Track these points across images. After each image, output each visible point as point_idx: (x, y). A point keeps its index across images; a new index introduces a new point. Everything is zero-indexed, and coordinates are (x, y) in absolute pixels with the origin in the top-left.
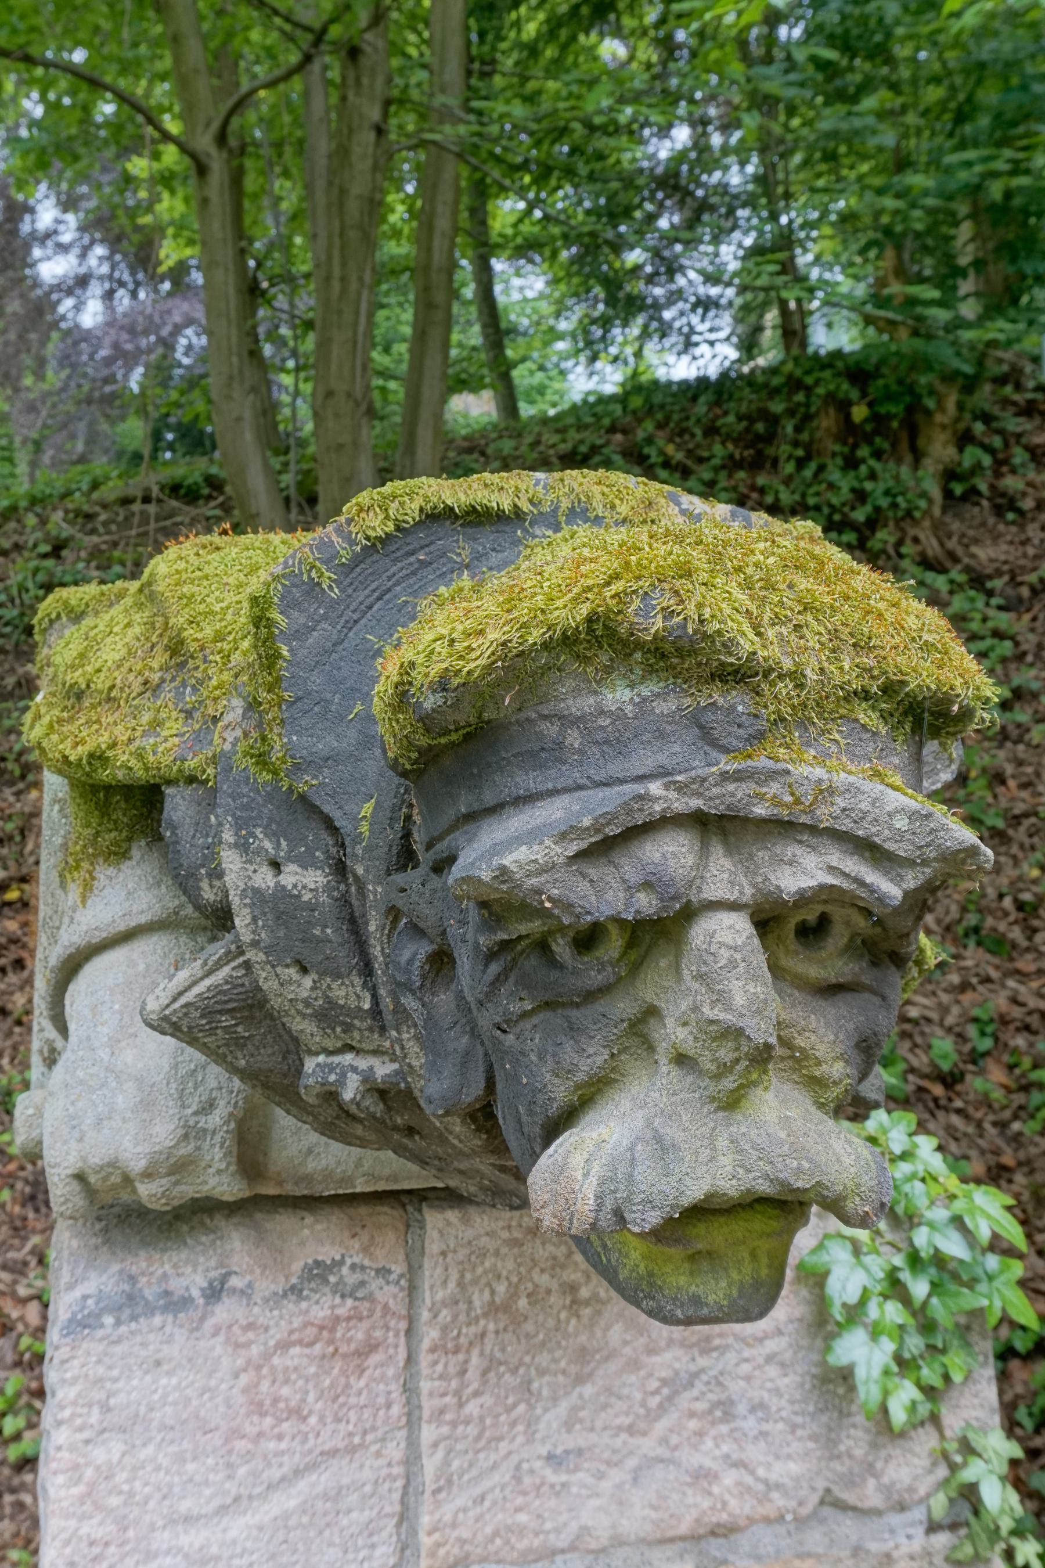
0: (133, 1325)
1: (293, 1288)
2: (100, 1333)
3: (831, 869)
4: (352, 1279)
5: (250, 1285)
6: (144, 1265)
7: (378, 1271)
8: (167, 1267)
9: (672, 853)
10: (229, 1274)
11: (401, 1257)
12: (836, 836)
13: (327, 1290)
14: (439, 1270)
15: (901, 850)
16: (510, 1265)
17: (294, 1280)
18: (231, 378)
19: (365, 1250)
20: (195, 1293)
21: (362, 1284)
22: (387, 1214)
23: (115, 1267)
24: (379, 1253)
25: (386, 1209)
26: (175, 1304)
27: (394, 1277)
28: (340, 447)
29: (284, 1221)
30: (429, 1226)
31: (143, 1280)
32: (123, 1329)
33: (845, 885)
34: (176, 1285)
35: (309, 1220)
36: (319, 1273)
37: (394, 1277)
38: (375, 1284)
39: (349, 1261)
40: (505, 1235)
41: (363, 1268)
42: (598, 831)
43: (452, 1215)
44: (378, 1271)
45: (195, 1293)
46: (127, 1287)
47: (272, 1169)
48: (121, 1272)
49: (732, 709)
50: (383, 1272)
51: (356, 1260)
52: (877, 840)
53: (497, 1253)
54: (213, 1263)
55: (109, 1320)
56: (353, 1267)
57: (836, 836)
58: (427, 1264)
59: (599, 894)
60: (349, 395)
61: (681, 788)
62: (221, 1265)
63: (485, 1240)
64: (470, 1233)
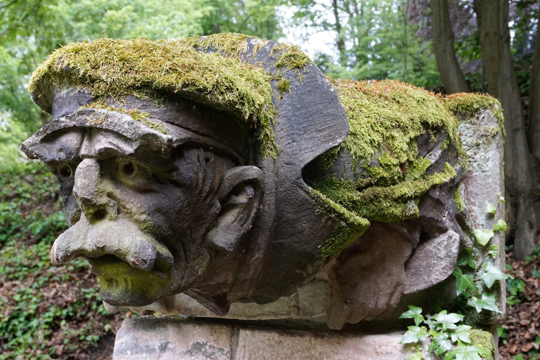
0: (136, 355)
1: (189, 351)
2: (126, 356)
3: (110, 143)
4: (210, 351)
5: (174, 348)
6: (140, 335)
7: (219, 349)
8: (148, 337)
9: (71, 140)
10: (168, 343)
11: (228, 345)
12: (113, 132)
13: (201, 353)
14: (242, 352)
15: (129, 135)
16: (269, 355)
17: (190, 348)
18: (440, 33)
19: (215, 341)
20: (157, 347)
21: (213, 353)
22: (225, 330)
23: (132, 334)
24: (221, 343)
25: (225, 327)
26: (150, 350)
27: (225, 352)
28: (492, 58)
29: (189, 327)
30: (240, 335)
31: (140, 340)
32: (133, 356)
33: (116, 148)
34: (150, 343)
35: (197, 327)
36: (198, 347)
37: (225, 352)
38: (218, 354)
39: (209, 344)
40: (267, 342)
41: (214, 347)
42: (45, 132)
43: (248, 332)
44: (219, 349)
45: (157, 347)
46: (135, 342)
47: (176, 304)
48: (133, 336)
49: (84, 93)
50: (221, 350)
51: (211, 344)
52: (120, 132)
53: (264, 349)
54: (163, 338)
55: (129, 352)
56: (210, 346)
57: (113, 132)
58: (238, 349)
59: (50, 153)
60: (496, 34)
61: (70, 118)
62: (165, 339)
63: (260, 343)
64: (254, 340)
